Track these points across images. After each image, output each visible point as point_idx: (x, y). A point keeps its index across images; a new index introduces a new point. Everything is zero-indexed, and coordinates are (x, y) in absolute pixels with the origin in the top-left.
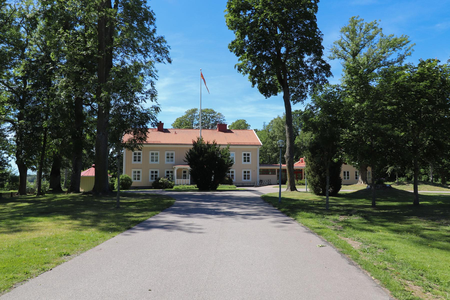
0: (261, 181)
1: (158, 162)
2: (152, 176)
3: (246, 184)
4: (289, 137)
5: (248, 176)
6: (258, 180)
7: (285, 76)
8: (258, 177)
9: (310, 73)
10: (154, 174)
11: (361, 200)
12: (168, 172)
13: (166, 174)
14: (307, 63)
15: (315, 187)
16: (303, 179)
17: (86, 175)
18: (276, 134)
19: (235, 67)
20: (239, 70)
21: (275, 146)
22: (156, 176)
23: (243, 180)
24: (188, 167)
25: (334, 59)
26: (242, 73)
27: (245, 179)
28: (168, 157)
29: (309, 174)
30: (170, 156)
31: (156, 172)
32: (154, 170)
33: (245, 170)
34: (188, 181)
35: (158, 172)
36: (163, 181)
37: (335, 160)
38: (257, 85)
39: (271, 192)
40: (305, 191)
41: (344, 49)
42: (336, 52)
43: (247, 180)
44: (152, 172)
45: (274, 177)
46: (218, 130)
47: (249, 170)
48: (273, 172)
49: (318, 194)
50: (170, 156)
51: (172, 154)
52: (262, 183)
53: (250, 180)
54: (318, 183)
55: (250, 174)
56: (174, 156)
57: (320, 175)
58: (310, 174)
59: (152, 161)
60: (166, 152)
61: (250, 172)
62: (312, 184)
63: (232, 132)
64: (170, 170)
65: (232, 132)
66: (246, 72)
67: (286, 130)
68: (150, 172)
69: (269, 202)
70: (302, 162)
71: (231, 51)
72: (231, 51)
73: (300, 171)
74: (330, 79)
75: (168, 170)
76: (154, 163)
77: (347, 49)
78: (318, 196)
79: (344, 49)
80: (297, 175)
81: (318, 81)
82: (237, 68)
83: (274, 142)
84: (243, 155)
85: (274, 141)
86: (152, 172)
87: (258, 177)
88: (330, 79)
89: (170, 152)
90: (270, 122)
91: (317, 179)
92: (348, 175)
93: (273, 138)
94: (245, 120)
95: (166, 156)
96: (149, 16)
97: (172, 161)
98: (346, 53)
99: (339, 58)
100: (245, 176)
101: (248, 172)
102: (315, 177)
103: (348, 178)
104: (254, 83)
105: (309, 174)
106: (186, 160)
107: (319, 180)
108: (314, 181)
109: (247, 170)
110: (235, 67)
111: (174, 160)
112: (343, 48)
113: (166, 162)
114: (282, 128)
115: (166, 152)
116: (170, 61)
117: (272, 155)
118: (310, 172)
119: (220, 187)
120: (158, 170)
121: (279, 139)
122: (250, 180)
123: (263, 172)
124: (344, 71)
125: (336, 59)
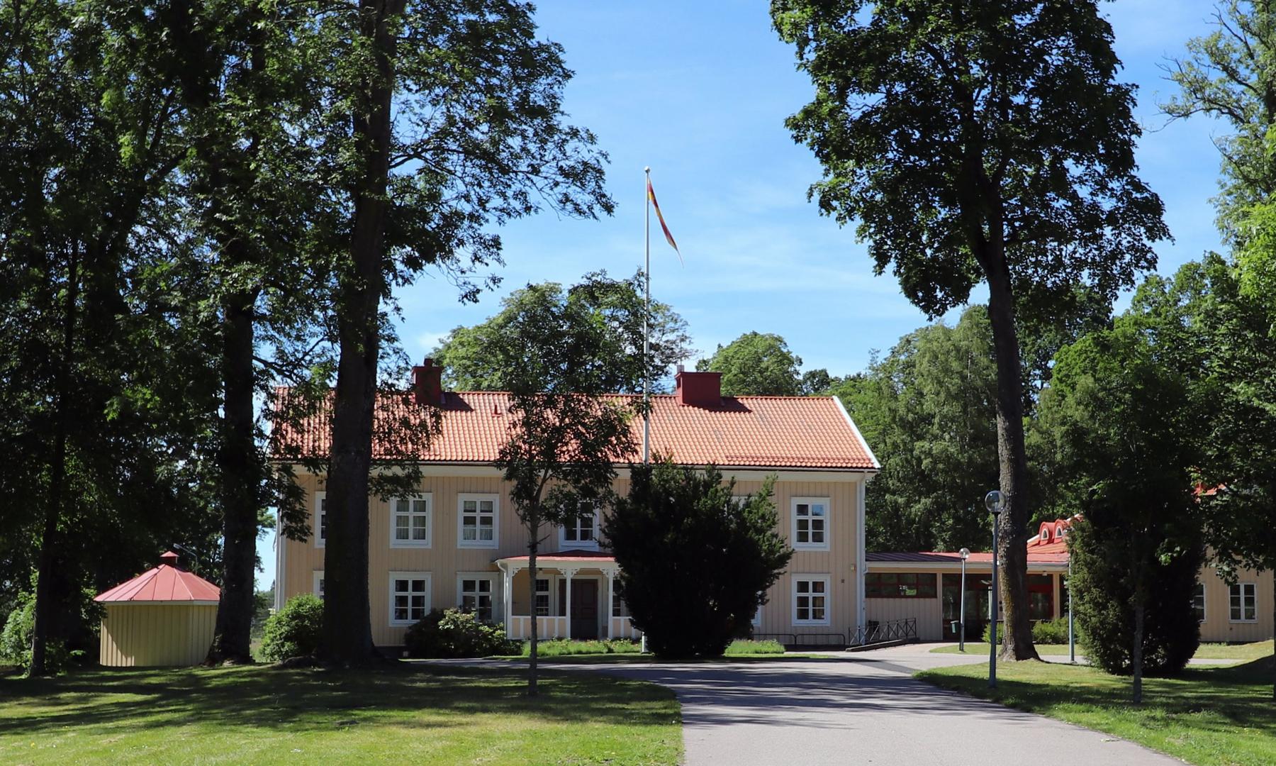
0: (873, 625)
1: (428, 543)
2: (401, 601)
3: (807, 641)
4: (1010, 460)
5: (818, 602)
6: (861, 620)
7: (996, 230)
8: (862, 607)
9: (1090, 220)
10: (410, 594)
11: (1257, 688)
12: (468, 585)
13: (460, 593)
14: (1076, 187)
15: (1103, 645)
16: (1056, 618)
17: (146, 596)
18: (928, 406)
19: (810, 195)
20: (825, 205)
21: (926, 462)
22: (418, 601)
23: (796, 622)
24: (609, 567)
25: (1186, 115)
26: (834, 214)
27: (803, 614)
28: (469, 521)
29: (1082, 598)
30: (478, 515)
31: (419, 585)
32: (410, 577)
33: (803, 579)
34: (562, 625)
35: (428, 586)
36: (454, 622)
37: (1163, 557)
38: (891, 266)
39: (944, 666)
40: (1069, 661)
41: (1232, 74)
42: (1197, 88)
43: (810, 622)
44: (402, 585)
45: (931, 609)
46: (680, 400)
47: (818, 579)
48: (924, 585)
49: (1117, 670)
50: (478, 515)
51: (488, 507)
52: (876, 636)
53: (826, 621)
54: (1115, 629)
55: (827, 594)
56: (495, 515)
57: (1123, 602)
58: (1087, 598)
59: (402, 535)
60: (462, 498)
61: (827, 587)
62: (1094, 633)
63: (742, 409)
64: (477, 578)
65: (742, 409)
66: (850, 212)
67: (1000, 432)
68: (392, 585)
69: (953, 689)
70: (1051, 541)
71: (798, 139)
72: (798, 139)
73: (1043, 583)
74: (1159, 247)
75: (469, 578)
76: (411, 544)
77: (1243, 72)
78: (1115, 677)
79: (1232, 74)
80: (1034, 599)
81: (1116, 255)
82: (817, 197)
83: (918, 444)
84: (794, 510)
85: (921, 438)
86: (402, 585)
87: (862, 607)
88: (1159, 247)
89: (479, 498)
90: (896, 343)
91: (1111, 614)
92: (1250, 601)
93: (916, 426)
94: (779, 340)
95: (461, 515)
96: (541, 62)
97: (489, 536)
98: (1239, 88)
99: (1208, 110)
100: (803, 602)
101: (818, 586)
102: (1105, 608)
103: (1250, 615)
104: (882, 259)
105: (1082, 598)
106: (607, 541)
107: (1119, 619)
108: (1102, 623)
109: (810, 579)
110: (810, 195)
111: (496, 534)
112: (1225, 69)
113: (461, 543)
114: (957, 381)
115: (462, 498)
116: (609, 208)
117: (908, 504)
118: (1089, 590)
119: (737, 648)
120: (427, 578)
121: (941, 427)
122: (826, 621)
123: (877, 586)
124: (1224, 171)
125: (1199, 117)
